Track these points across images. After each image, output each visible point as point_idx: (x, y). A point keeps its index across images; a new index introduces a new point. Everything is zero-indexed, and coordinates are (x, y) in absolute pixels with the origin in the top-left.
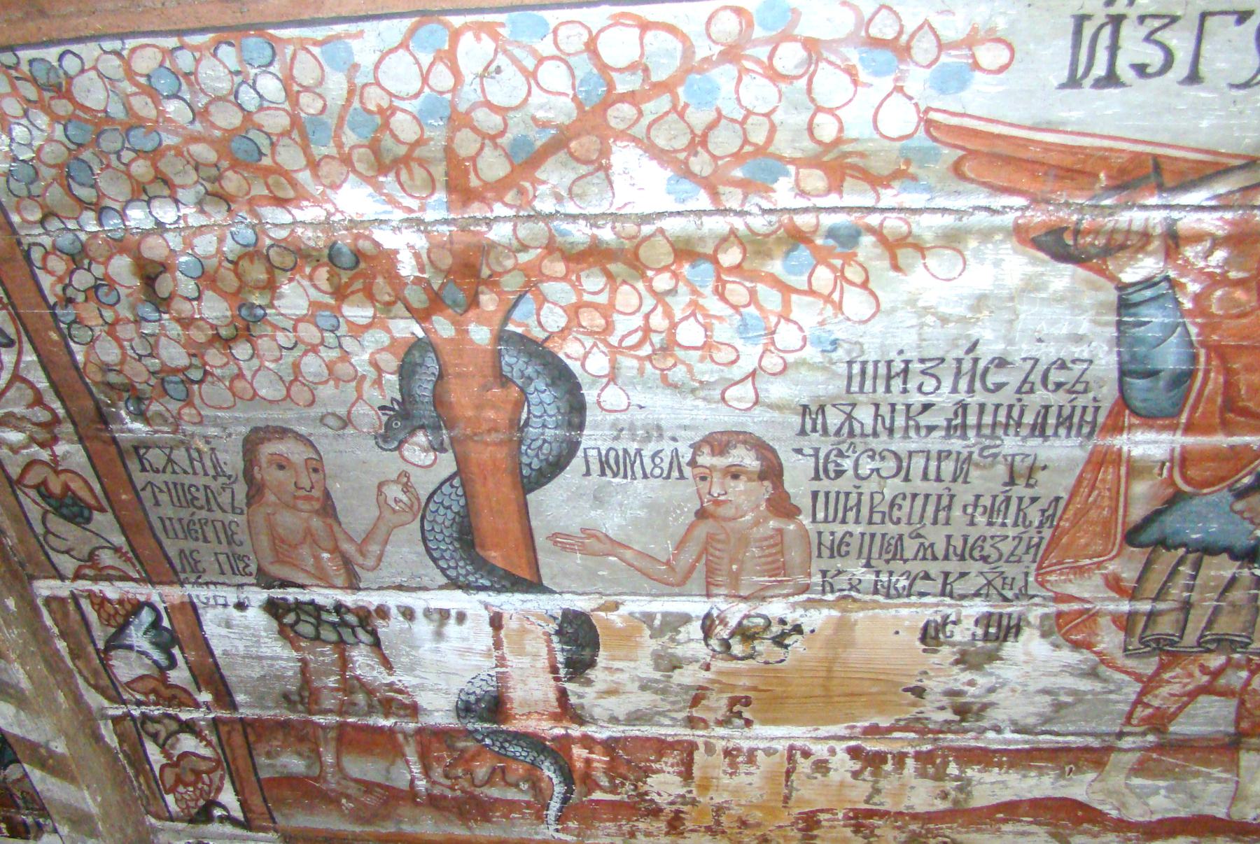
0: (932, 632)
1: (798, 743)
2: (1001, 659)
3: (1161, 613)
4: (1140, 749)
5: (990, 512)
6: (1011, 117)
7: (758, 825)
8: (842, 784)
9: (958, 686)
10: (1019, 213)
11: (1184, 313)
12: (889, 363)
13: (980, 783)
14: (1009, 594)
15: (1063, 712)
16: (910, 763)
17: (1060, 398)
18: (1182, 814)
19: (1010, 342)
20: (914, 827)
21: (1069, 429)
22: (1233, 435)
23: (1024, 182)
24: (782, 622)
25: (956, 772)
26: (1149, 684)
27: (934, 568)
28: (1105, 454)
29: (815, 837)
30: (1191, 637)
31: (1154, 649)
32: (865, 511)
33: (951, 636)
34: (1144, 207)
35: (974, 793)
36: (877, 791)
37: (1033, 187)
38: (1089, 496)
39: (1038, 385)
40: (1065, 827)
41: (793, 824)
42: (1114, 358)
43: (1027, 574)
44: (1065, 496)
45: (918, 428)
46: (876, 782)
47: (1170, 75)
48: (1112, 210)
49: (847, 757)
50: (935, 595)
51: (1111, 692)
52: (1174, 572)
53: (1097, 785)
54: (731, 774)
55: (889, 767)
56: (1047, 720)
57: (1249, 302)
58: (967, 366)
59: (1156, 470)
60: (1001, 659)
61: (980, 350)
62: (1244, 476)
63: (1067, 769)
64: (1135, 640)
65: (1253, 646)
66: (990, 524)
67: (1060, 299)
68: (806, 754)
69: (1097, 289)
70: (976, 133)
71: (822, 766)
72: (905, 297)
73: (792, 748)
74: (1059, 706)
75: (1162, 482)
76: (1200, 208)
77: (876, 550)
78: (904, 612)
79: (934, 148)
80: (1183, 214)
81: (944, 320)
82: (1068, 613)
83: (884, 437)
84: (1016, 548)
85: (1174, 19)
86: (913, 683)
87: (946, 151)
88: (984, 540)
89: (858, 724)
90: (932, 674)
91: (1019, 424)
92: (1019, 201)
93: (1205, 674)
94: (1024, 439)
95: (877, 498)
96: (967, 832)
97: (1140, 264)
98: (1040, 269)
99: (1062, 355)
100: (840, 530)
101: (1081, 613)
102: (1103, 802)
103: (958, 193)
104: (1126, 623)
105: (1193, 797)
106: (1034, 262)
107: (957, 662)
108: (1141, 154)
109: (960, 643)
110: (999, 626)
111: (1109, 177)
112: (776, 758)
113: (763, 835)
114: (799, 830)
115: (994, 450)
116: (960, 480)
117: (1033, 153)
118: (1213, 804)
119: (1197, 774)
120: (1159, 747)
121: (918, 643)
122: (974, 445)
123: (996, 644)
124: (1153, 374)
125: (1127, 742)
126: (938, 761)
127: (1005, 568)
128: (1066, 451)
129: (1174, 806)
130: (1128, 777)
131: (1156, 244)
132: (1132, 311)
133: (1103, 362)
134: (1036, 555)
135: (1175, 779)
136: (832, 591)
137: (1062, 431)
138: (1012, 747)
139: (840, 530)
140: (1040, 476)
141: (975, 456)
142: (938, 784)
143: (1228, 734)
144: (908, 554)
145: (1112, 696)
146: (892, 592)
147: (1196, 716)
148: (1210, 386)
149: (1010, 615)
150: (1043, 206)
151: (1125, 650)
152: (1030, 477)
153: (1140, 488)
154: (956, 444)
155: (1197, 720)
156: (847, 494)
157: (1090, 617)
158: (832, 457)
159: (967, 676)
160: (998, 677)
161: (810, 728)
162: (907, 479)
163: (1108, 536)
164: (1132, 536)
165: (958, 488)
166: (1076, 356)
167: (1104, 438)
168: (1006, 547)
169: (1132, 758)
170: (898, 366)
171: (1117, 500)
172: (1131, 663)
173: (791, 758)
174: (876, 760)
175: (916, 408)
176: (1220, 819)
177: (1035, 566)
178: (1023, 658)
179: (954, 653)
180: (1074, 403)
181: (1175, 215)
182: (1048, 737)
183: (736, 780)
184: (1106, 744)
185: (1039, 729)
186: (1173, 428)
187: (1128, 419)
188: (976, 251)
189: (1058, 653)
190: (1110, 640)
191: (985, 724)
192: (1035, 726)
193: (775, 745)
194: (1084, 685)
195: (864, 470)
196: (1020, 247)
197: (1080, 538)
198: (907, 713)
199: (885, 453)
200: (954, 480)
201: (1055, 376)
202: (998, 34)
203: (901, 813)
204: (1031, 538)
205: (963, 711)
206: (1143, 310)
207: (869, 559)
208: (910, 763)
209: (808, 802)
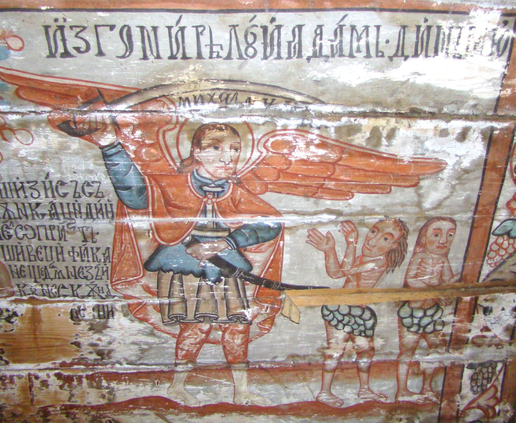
0: (75, 314)
1: (32, 372)
2: (109, 327)
3: (174, 304)
4: (187, 371)
5: (80, 254)
6: (32, 70)
7: (21, 415)
8: (56, 392)
9: (95, 341)
10: (48, 114)
11: (132, 160)
12: (14, 183)
13: (118, 390)
14: (103, 295)
15: (146, 353)
16: (84, 380)
17: (92, 200)
18: (214, 403)
19: (62, 173)
20: (93, 413)
21: (103, 214)
22: (175, 217)
23: (47, 100)
24: (7, 310)
25: (106, 385)
26: (180, 339)
27: (66, 283)
28: (122, 226)
29: (49, 420)
30: (191, 316)
31: (176, 322)
32: (26, 255)
33: (84, 316)
34: (99, 111)
35: (117, 395)
36: (72, 395)
37: (52, 103)
38: (121, 247)
39: (82, 194)
40: (162, 410)
41: (38, 413)
42: (109, 181)
43: (107, 285)
44: (111, 246)
45: (37, 215)
46: (71, 391)
47: (91, 52)
48: (86, 112)
49: (56, 378)
50: (71, 296)
51: (163, 343)
52: (172, 283)
53: (171, 390)
54: (4, 389)
55: (75, 383)
56: (141, 358)
57: (158, 154)
58: (48, 185)
59: (147, 234)
60: (109, 327)
61: (51, 177)
62: (187, 237)
63: (156, 382)
64: (166, 317)
65: (220, 319)
66: (83, 261)
67: (77, 154)
68: (37, 378)
69: (92, 148)
70: (21, 78)
71: (45, 383)
72: (12, 153)
73: (29, 375)
74: (143, 351)
75: (152, 240)
76: (124, 112)
77: (37, 274)
78: (60, 305)
79: (4, 85)
80: (117, 114)
81: (31, 163)
82: (133, 304)
83: (24, 219)
84: (98, 272)
85: (84, 28)
86: (74, 340)
87: (10, 86)
88: (83, 269)
89: (57, 362)
90: (81, 335)
91: (80, 213)
92: (48, 109)
93: (203, 333)
94: (85, 220)
95: (29, 247)
96: (118, 415)
97: (106, 137)
98: (65, 139)
99: (86, 179)
100: (19, 264)
101: (140, 304)
102: (176, 398)
103: (21, 105)
104: (160, 308)
105: (216, 394)
106: (61, 136)
107: (90, 329)
108: (92, 87)
109: (89, 320)
110: (104, 311)
111: (82, 98)
112: (23, 380)
113: (25, 420)
114: (42, 417)
115: (72, 225)
116: (63, 239)
117: (45, 87)
118: (225, 397)
119: (215, 383)
120: (195, 370)
121: (70, 320)
122: (64, 222)
123: (105, 320)
124: (129, 188)
125: (179, 368)
126: (97, 379)
127: (97, 282)
128: (104, 225)
129: (209, 399)
130: (184, 385)
131: (110, 128)
132: (110, 158)
133: (105, 182)
134: (107, 276)
135: (206, 385)
136: (25, 295)
137: (100, 216)
138: (129, 372)
139: (19, 264)
140: (97, 237)
141: (66, 228)
142: (99, 390)
143: (224, 363)
144: (52, 276)
145: (165, 345)
146: (51, 295)
147: (206, 354)
148: (156, 195)
149: (107, 306)
150: (58, 111)
151: (163, 322)
152: (93, 238)
153: (142, 243)
154: (55, 222)
155: (208, 356)
156: (16, 247)
157: (143, 306)
158: (5, 229)
159: (96, 336)
160: (111, 336)
161: (36, 364)
162: (39, 239)
163: (136, 266)
164: (147, 265)
165: (63, 243)
166: (93, 180)
167: (119, 219)
168: (94, 272)
169: (184, 376)
170: (19, 185)
171: (134, 247)
172: (167, 328)
173: (30, 379)
174: (69, 380)
175: (34, 205)
176: (231, 404)
177: (109, 281)
178: (120, 327)
179: (88, 325)
180: (101, 202)
181: (114, 114)
182: (144, 366)
183: (6, 393)
184: (170, 369)
185: (138, 362)
186: (147, 214)
187: (127, 210)
188: (36, 132)
189: (133, 324)
190: (155, 317)
191: (113, 360)
192: (136, 361)
193: (21, 373)
194: (151, 340)
195: (21, 234)
196: (54, 130)
197: (124, 267)
198: (76, 355)
199: (27, 227)
200: (60, 239)
201: (87, 190)
202: (15, 34)
203: (85, 406)
204: (103, 268)
205: (100, 353)
206: (114, 158)
207: (35, 278)
208: (84, 380)
209: (43, 402)
